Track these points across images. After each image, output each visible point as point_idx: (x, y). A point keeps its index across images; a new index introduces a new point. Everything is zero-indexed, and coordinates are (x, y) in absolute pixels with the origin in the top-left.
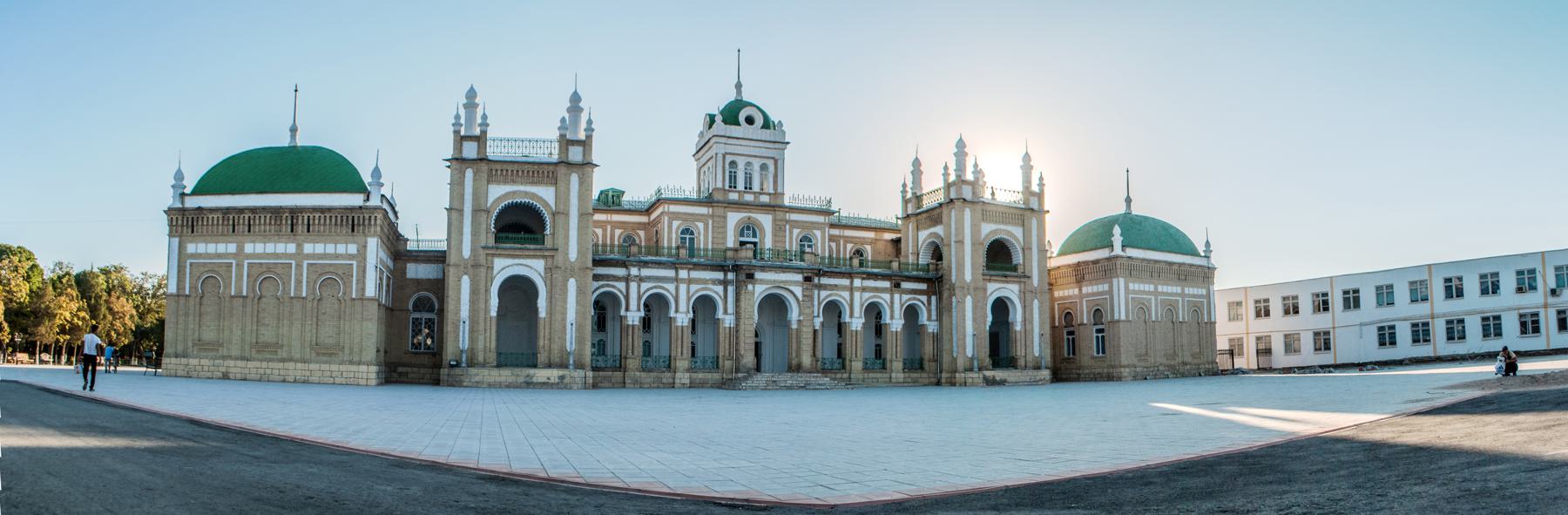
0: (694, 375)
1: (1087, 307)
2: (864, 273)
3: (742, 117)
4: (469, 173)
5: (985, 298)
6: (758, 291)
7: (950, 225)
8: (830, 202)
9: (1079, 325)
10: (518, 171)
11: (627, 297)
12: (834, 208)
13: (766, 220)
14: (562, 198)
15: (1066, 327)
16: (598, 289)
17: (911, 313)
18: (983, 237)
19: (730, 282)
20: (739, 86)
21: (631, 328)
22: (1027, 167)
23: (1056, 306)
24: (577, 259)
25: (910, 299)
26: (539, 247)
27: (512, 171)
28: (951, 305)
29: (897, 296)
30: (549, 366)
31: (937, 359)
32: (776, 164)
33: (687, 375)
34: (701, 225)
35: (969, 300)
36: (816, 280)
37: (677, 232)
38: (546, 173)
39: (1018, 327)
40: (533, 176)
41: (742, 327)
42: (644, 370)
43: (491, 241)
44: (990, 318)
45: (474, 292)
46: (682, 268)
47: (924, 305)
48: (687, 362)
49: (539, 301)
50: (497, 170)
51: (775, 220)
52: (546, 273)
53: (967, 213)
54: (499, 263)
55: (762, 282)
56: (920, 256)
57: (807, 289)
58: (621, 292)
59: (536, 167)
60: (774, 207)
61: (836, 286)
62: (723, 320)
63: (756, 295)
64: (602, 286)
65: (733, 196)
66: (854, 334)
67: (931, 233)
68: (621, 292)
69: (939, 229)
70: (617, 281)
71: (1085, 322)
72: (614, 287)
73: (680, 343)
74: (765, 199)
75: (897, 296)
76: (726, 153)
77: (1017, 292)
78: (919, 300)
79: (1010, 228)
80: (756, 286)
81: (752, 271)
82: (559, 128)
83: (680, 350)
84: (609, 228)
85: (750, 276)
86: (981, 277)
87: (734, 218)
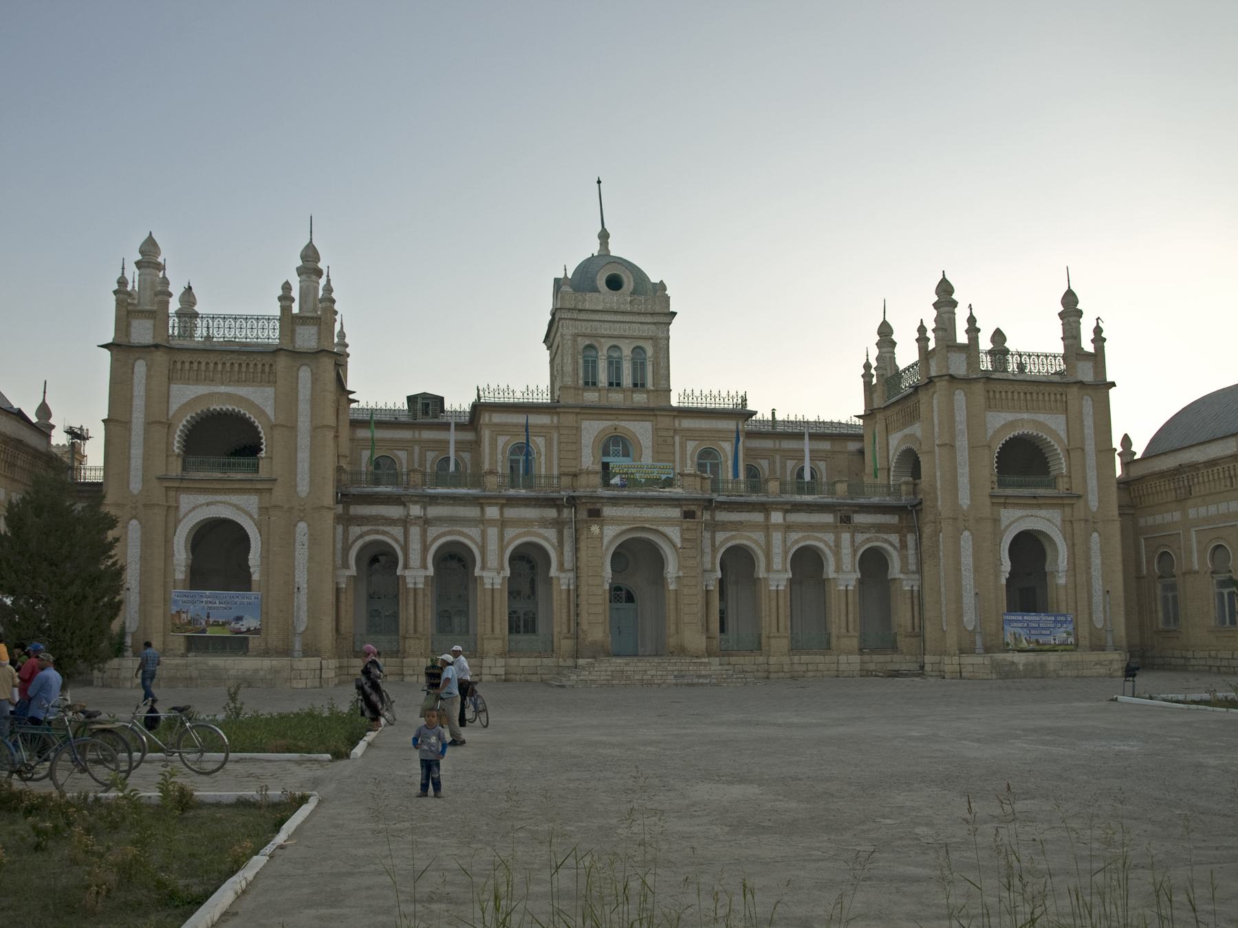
0: (513, 662)
1: (1199, 542)
2: (786, 503)
4: (140, 367)
5: (997, 535)
6: (609, 534)
7: (933, 419)
8: (744, 400)
9: (1184, 574)
12: (750, 407)
13: (642, 430)
14: (288, 402)
15: (1161, 577)
16: (361, 536)
17: (873, 562)
18: (990, 432)
19: (567, 523)
20: (604, 236)
21: (411, 595)
22: (1070, 310)
25: (868, 540)
26: (250, 476)
27: (207, 363)
28: (938, 546)
29: (846, 537)
31: (918, 633)
32: (656, 346)
33: (501, 662)
36: (707, 516)
37: (503, 453)
38: (260, 366)
39: (1062, 581)
41: (583, 590)
43: (176, 468)
44: (1007, 566)
45: (146, 543)
46: (491, 505)
47: (895, 548)
48: (500, 643)
49: (251, 556)
50: (183, 362)
51: (656, 430)
52: (260, 515)
55: (614, 521)
56: (892, 473)
57: (688, 529)
58: (397, 541)
59: (244, 358)
60: (653, 410)
61: (741, 523)
62: (558, 579)
63: (606, 541)
64: (368, 533)
65: (591, 397)
66: (774, 595)
67: (906, 436)
68: (397, 541)
69: (916, 429)
70: (390, 525)
71: (1196, 567)
74: (640, 398)
75: (846, 537)
77: (1059, 523)
78: (886, 541)
80: (605, 528)
81: (598, 506)
82: (280, 299)
83: (489, 625)
84: (417, 449)
85: (595, 514)
86: (987, 501)
87: (592, 429)
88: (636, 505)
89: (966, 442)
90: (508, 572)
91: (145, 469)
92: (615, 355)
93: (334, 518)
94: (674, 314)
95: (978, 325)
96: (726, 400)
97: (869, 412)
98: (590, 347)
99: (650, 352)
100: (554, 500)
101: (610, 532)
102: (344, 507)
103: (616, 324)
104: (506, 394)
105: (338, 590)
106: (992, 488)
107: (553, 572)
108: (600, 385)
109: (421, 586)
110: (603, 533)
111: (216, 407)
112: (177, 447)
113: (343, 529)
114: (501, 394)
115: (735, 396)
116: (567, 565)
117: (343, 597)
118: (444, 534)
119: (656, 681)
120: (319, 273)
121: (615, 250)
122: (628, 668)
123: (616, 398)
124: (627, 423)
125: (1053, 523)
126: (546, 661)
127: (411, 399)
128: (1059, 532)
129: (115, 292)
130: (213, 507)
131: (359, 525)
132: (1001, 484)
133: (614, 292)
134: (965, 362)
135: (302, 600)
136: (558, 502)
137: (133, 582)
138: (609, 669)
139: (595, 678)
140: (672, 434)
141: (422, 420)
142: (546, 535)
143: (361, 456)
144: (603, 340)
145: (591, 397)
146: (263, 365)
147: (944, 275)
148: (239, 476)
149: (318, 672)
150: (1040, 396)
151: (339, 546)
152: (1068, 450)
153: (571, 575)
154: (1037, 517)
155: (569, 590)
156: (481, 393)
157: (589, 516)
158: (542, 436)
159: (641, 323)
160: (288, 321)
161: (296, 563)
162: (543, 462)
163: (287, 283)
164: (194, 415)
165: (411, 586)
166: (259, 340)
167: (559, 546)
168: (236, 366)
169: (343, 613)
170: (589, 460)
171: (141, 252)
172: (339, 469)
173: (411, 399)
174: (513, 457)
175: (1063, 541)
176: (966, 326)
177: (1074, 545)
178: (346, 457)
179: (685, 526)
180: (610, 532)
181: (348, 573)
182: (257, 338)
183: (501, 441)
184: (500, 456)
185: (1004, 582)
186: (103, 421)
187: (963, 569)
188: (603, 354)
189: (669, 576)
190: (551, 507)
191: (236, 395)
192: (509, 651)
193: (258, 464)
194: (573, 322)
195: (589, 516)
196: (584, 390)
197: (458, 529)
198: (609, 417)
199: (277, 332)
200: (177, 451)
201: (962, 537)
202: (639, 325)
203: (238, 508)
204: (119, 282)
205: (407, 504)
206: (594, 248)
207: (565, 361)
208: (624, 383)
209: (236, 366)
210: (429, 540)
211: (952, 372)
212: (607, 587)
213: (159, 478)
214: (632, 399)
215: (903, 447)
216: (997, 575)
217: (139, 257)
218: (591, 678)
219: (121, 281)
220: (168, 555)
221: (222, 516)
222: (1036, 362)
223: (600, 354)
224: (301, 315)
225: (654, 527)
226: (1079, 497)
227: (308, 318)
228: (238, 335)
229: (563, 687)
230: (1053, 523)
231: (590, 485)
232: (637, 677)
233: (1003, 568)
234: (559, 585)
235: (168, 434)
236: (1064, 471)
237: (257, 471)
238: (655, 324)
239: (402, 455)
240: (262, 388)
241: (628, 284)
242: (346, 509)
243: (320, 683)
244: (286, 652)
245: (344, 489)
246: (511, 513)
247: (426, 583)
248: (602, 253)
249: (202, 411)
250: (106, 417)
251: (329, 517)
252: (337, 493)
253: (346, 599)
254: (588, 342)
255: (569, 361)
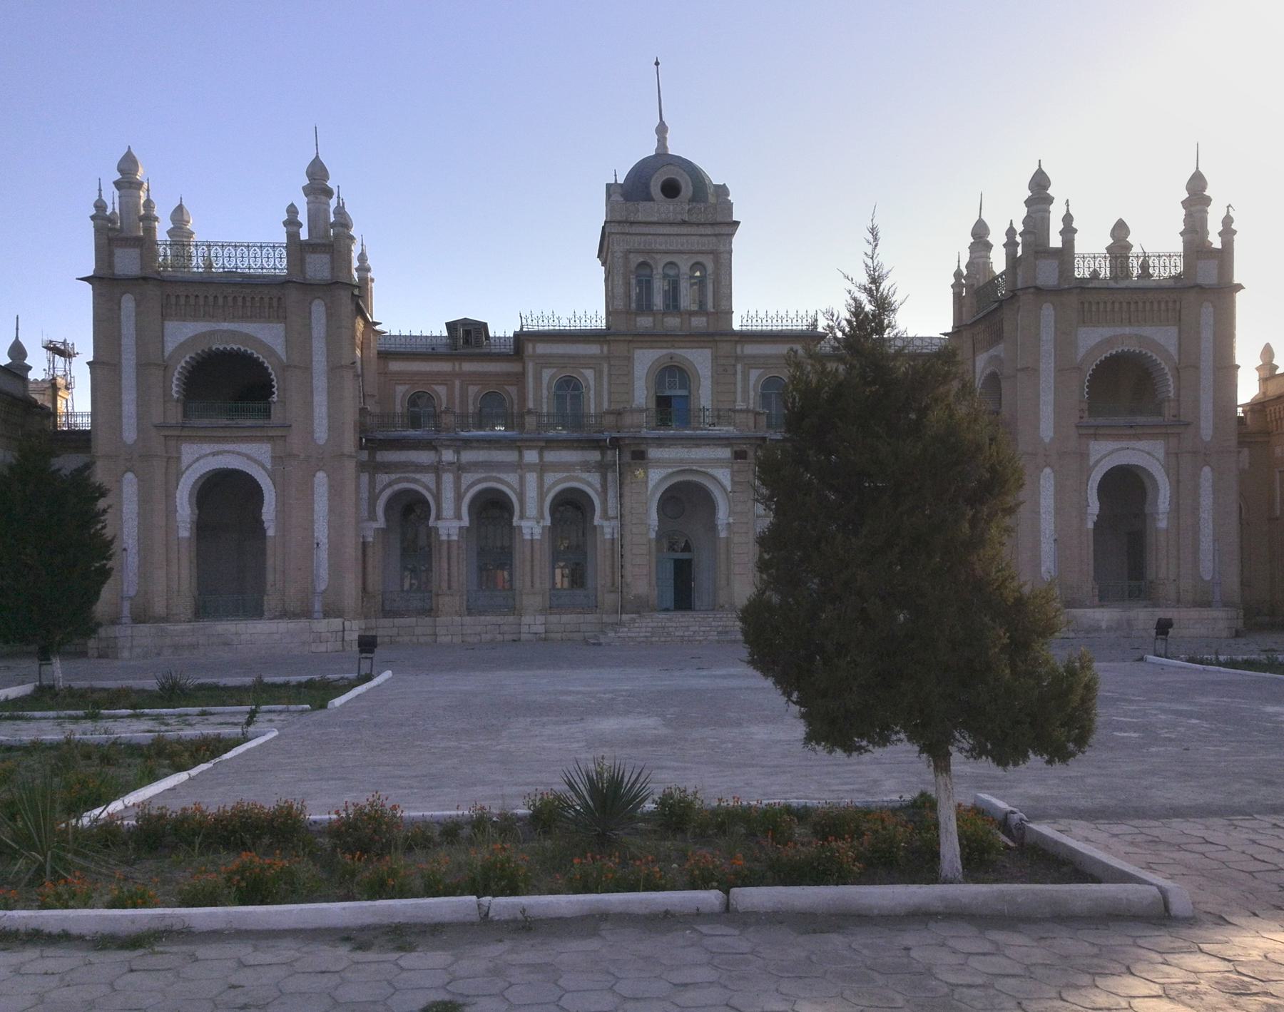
0: (553, 618)
3: (656, 190)
4: (128, 303)
6: (655, 479)
10: (216, 297)
11: (521, 496)
16: (390, 485)
20: (662, 130)
23: (1278, 476)
24: (327, 440)
26: (261, 422)
30: (285, 614)
33: (540, 619)
34: (589, 374)
35: (1047, 481)
37: (549, 388)
38: (266, 300)
39: (1163, 524)
40: (244, 306)
42: (470, 612)
43: (175, 415)
44: (1094, 507)
46: (529, 448)
49: (264, 510)
51: (715, 358)
53: (319, 310)
54: (189, 451)
55: (660, 463)
58: (428, 489)
59: (248, 291)
60: (712, 335)
63: (651, 485)
65: (645, 322)
68: (428, 489)
69: (999, 350)
70: (421, 472)
72: (416, 481)
73: (528, 568)
74: (699, 323)
76: (629, 252)
79: (250, 328)
81: (643, 447)
82: (285, 224)
83: (528, 579)
84: (457, 383)
85: (640, 456)
88: (683, 446)
89: (1052, 365)
90: (548, 522)
91: (140, 417)
92: (672, 272)
93: (356, 466)
94: (737, 223)
95: (1075, 225)
96: (794, 321)
97: (956, 329)
98: (644, 264)
99: (710, 267)
100: (598, 441)
101: (655, 475)
102: (369, 454)
103: (672, 238)
104: (551, 321)
105: (364, 544)
106: (1081, 418)
107: (597, 521)
108: (655, 308)
109: (455, 538)
110: (647, 477)
111: (218, 346)
112: (175, 391)
113: (370, 478)
114: (546, 321)
115: (804, 316)
116: (611, 513)
117: (370, 552)
118: (479, 481)
119: (698, 638)
120: (328, 193)
121: (673, 150)
122: (670, 624)
123: (672, 322)
124: (684, 350)
125: (1153, 456)
126: (589, 618)
127: (450, 326)
128: (1160, 467)
129: (93, 218)
130: (220, 457)
131: (386, 473)
132: (1093, 411)
133: (670, 200)
134: (1057, 270)
135: (323, 555)
136: (601, 444)
137: (130, 541)
138: (650, 624)
139: (634, 635)
140: (733, 362)
141: (462, 351)
142: (590, 479)
143: (395, 392)
144: (658, 256)
145: (645, 322)
146: (271, 299)
147: (1040, 166)
148: (249, 423)
149: (340, 634)
150: (1148, 305)
151: (365, 495)
152: (1177, 369)
153: (616, 523)
154: (1134, 449)
155: (613, 539)
156: (524, 321)
157: (633, 459)
158: (591, 368)
159: (701, 235)
160: (296, 248)
161: (315, 517)
162: (592, 397)
163: (292, 205)
164: (193, 355)
165: (444, 538)
166: (265, 271)
167: (602, 492)
168: (240, 300)
169: (370, 569)
170: (642, 395)
171: (120, 170)
172: (363, 411)
173: (450, 326)
174: (560, 393)
175: (1165, 477)
176: (1061, 226)
177: (1178, 482)
178: (374, 396)
179: (736, 467)
180: (655, 475)
181: (375, 525)
182: (262, 269)
183: (547, 374)
184: (545, 392)
185: (1090, 525)
186: (88, 363)
187: (1042, 511)
188: (658, 271)
189: (719, 522)
190: (594, 448)
191: (241, 332)
192: (550, 608)
193: (270, 409)
194: (624, 237)
195: (633, 459)
196: (637, 314)
197: (494, 474)
198: (665, 345)
199: (285, 261)
200: (176, 396)
201: (1042, 475)
202: (698, 238)
203: (249, 457)
204: (96, 206)
205: (439, 448)
206: (650, 150)
207: (616, 283)
208: (682, 306)
209: (240, 300)
210: (463, 487)
211: (1039, 283)
212: (653, 535)
213: (156, 426)
214: (690, 323)
215: (988, 371)
216: (1082, 516)
217: (118, 176)
218: (629, 634)
219: (98, 205)
220: (171, 511)
221: (230, 467)
222: (1167, 264)
223: (655, 272)
224: (312, 242)
225: (703, 469)
226: (1187, 424)
227: (318, 245)
228: (240, 265)
229: (600, 644)
230: (1153, 456)
231: (641, 424)
232: (677, 634)
233: (1090, 510)
234: (603, 534)
235: (164, 377)
236: (1171, 394)
237: (269, 417)
238: (716, 235)
239: (441, 390)
240: (271, 325)
241: (687, 190)
242: (372, 456)
243: (343, 646)
244: (307, 614)
245: (369, 434)
246: (551, 456)
247: (460, 535)
248: (660, 151)
249: (203, 351)
250: (91, 359)
251: (350, 466)
252: (361, 439)
253: (374, 553)
254: (641, 260)
255: (620, 283)
